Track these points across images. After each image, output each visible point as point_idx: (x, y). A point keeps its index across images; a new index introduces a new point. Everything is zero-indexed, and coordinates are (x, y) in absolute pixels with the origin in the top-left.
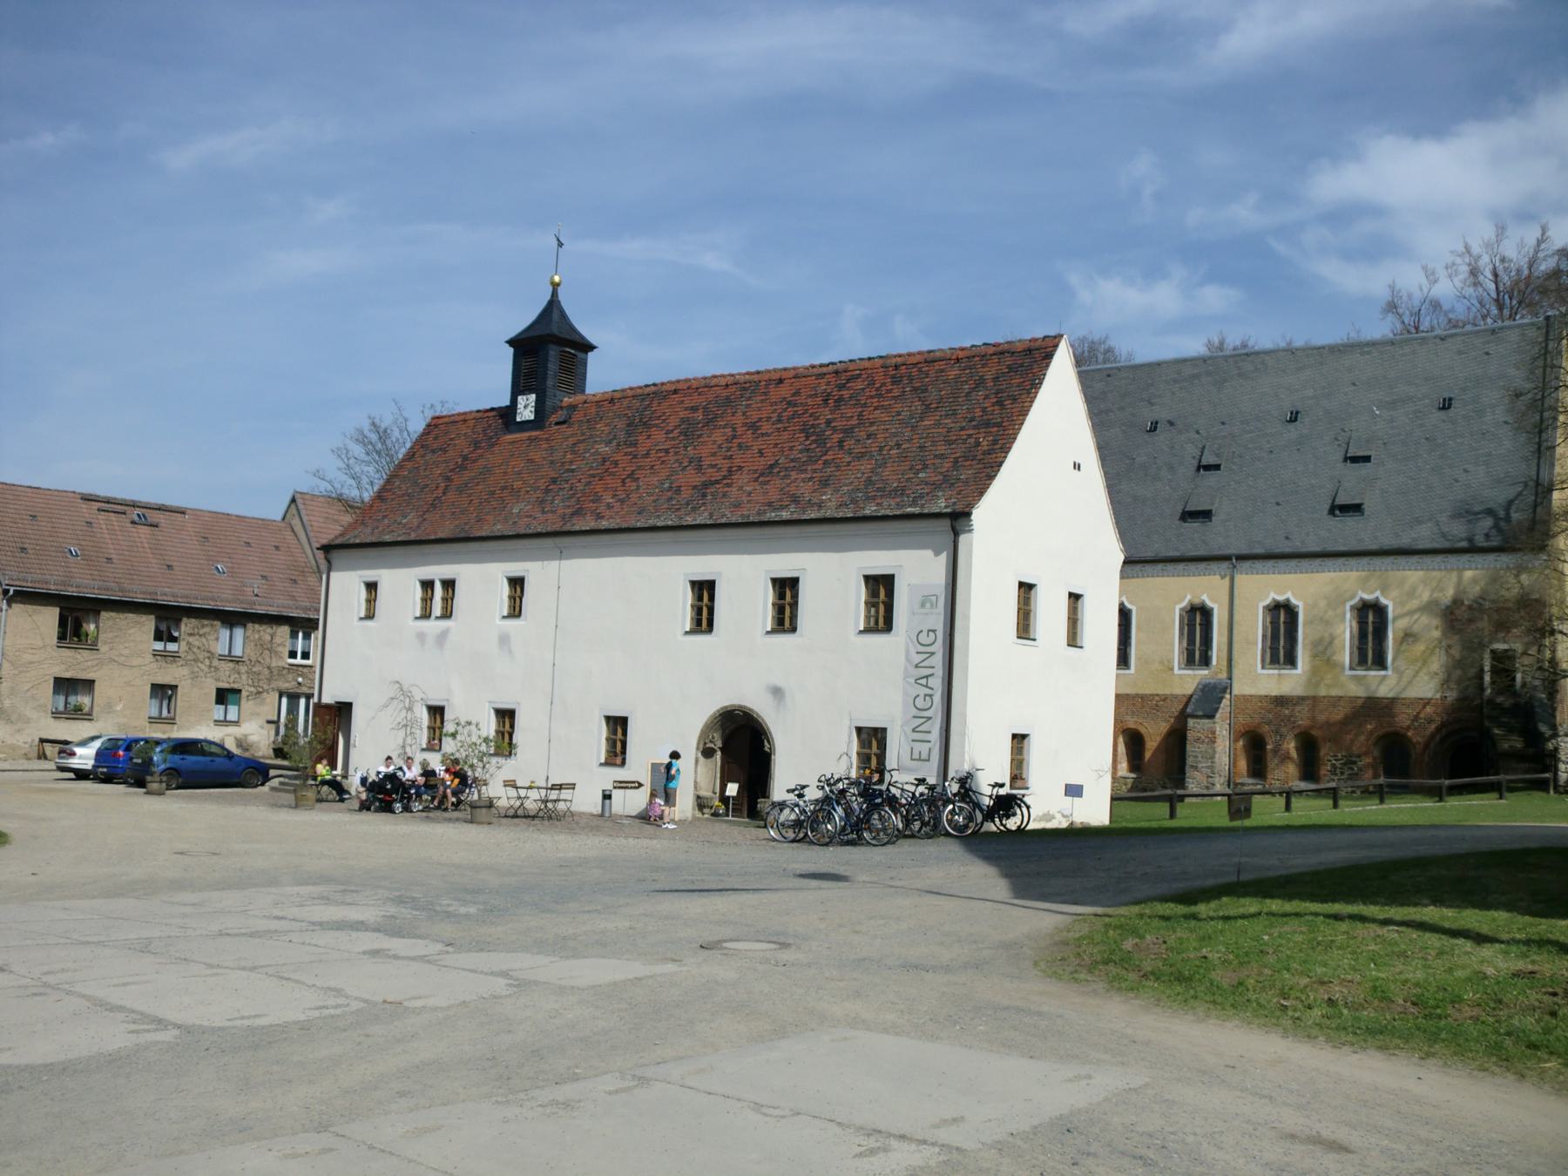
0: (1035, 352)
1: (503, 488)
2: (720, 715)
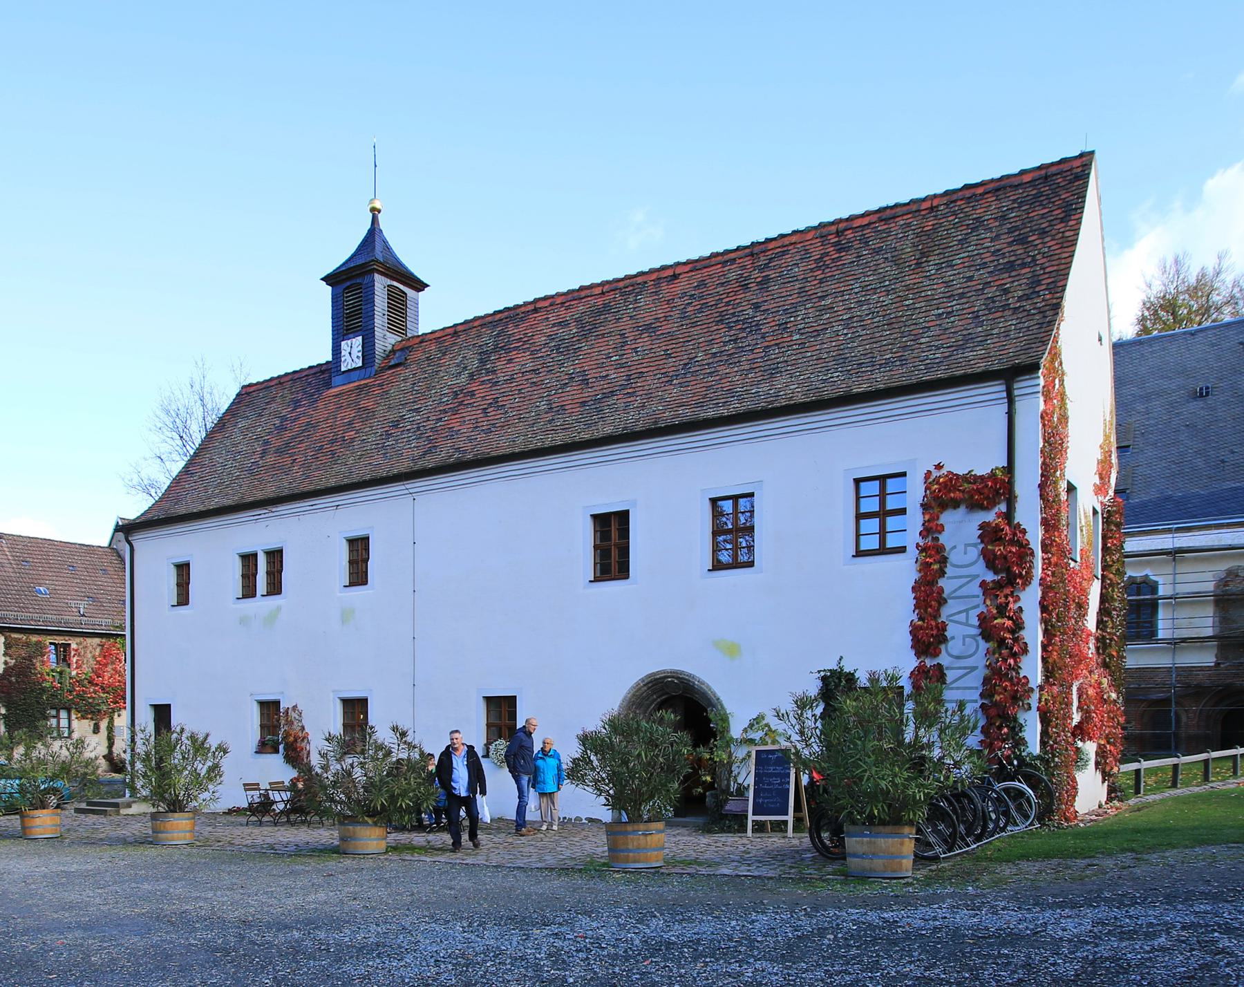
1: (333, 442)
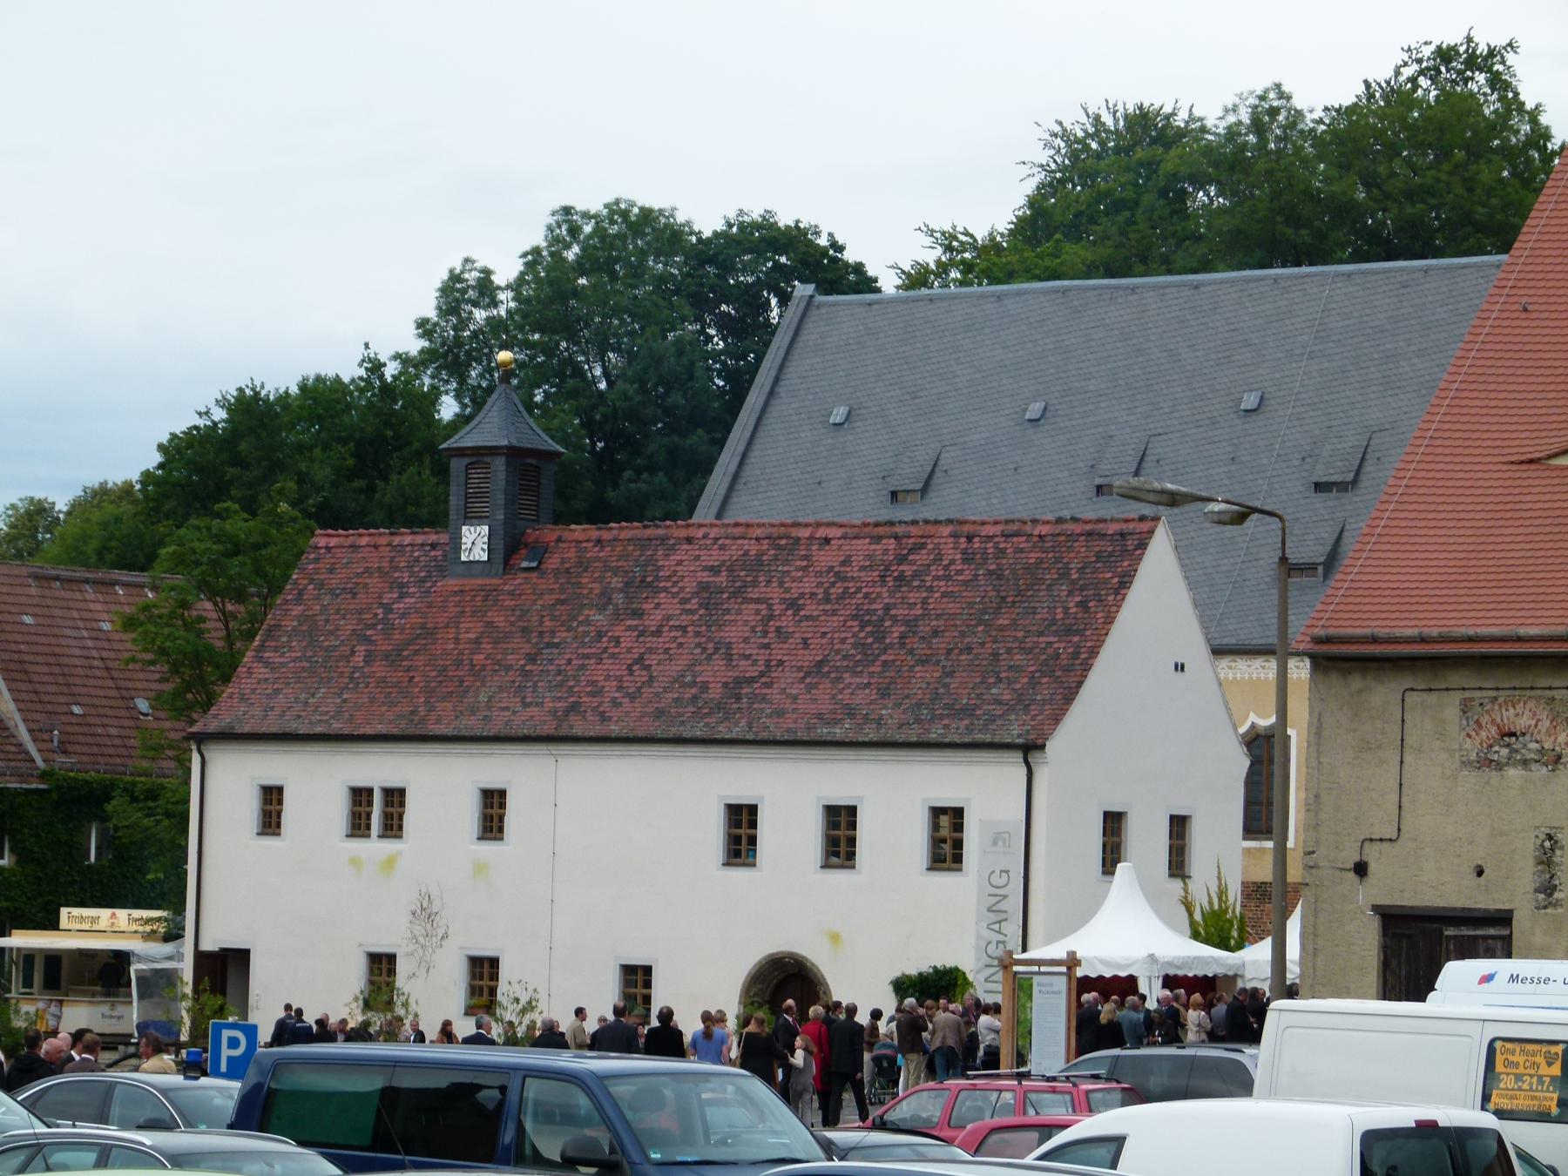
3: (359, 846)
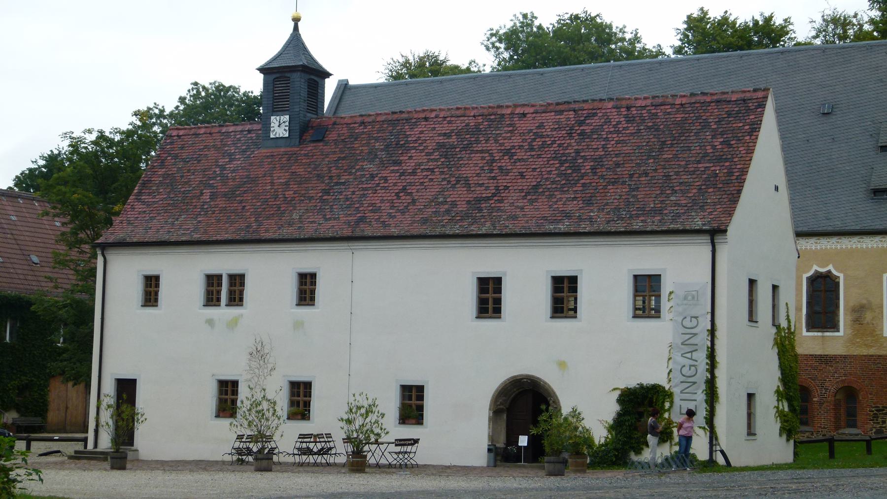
0: (748, 102)
2: (510, 383)
3: (212, 312)
